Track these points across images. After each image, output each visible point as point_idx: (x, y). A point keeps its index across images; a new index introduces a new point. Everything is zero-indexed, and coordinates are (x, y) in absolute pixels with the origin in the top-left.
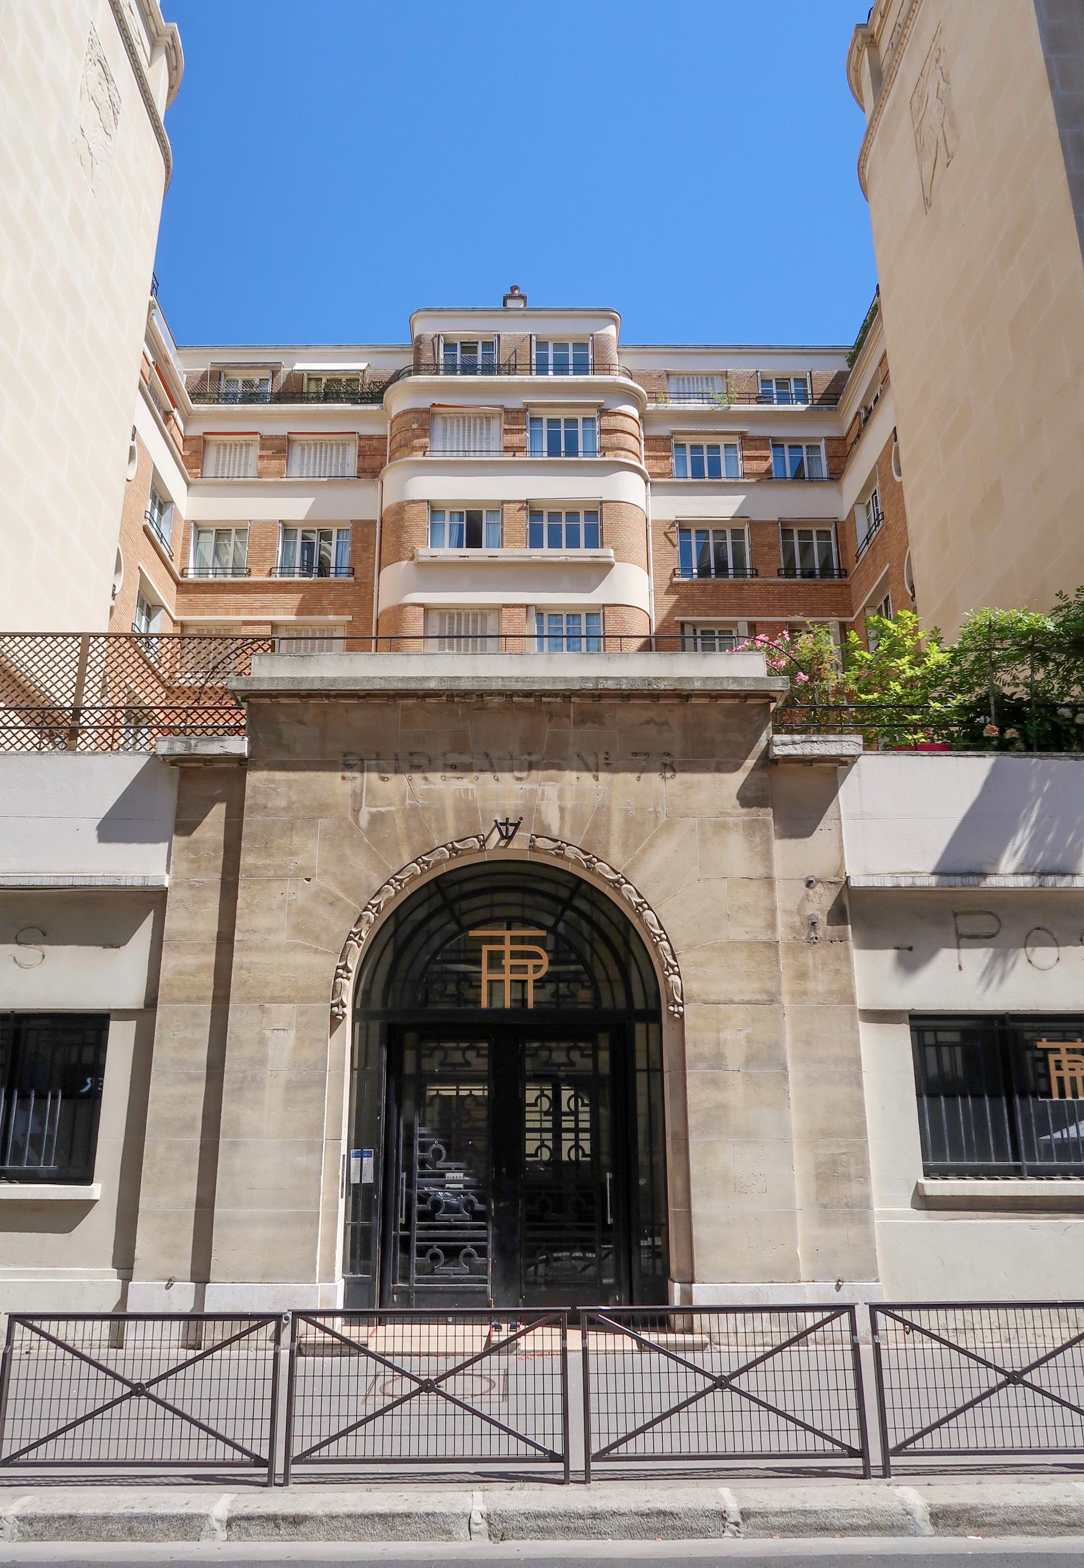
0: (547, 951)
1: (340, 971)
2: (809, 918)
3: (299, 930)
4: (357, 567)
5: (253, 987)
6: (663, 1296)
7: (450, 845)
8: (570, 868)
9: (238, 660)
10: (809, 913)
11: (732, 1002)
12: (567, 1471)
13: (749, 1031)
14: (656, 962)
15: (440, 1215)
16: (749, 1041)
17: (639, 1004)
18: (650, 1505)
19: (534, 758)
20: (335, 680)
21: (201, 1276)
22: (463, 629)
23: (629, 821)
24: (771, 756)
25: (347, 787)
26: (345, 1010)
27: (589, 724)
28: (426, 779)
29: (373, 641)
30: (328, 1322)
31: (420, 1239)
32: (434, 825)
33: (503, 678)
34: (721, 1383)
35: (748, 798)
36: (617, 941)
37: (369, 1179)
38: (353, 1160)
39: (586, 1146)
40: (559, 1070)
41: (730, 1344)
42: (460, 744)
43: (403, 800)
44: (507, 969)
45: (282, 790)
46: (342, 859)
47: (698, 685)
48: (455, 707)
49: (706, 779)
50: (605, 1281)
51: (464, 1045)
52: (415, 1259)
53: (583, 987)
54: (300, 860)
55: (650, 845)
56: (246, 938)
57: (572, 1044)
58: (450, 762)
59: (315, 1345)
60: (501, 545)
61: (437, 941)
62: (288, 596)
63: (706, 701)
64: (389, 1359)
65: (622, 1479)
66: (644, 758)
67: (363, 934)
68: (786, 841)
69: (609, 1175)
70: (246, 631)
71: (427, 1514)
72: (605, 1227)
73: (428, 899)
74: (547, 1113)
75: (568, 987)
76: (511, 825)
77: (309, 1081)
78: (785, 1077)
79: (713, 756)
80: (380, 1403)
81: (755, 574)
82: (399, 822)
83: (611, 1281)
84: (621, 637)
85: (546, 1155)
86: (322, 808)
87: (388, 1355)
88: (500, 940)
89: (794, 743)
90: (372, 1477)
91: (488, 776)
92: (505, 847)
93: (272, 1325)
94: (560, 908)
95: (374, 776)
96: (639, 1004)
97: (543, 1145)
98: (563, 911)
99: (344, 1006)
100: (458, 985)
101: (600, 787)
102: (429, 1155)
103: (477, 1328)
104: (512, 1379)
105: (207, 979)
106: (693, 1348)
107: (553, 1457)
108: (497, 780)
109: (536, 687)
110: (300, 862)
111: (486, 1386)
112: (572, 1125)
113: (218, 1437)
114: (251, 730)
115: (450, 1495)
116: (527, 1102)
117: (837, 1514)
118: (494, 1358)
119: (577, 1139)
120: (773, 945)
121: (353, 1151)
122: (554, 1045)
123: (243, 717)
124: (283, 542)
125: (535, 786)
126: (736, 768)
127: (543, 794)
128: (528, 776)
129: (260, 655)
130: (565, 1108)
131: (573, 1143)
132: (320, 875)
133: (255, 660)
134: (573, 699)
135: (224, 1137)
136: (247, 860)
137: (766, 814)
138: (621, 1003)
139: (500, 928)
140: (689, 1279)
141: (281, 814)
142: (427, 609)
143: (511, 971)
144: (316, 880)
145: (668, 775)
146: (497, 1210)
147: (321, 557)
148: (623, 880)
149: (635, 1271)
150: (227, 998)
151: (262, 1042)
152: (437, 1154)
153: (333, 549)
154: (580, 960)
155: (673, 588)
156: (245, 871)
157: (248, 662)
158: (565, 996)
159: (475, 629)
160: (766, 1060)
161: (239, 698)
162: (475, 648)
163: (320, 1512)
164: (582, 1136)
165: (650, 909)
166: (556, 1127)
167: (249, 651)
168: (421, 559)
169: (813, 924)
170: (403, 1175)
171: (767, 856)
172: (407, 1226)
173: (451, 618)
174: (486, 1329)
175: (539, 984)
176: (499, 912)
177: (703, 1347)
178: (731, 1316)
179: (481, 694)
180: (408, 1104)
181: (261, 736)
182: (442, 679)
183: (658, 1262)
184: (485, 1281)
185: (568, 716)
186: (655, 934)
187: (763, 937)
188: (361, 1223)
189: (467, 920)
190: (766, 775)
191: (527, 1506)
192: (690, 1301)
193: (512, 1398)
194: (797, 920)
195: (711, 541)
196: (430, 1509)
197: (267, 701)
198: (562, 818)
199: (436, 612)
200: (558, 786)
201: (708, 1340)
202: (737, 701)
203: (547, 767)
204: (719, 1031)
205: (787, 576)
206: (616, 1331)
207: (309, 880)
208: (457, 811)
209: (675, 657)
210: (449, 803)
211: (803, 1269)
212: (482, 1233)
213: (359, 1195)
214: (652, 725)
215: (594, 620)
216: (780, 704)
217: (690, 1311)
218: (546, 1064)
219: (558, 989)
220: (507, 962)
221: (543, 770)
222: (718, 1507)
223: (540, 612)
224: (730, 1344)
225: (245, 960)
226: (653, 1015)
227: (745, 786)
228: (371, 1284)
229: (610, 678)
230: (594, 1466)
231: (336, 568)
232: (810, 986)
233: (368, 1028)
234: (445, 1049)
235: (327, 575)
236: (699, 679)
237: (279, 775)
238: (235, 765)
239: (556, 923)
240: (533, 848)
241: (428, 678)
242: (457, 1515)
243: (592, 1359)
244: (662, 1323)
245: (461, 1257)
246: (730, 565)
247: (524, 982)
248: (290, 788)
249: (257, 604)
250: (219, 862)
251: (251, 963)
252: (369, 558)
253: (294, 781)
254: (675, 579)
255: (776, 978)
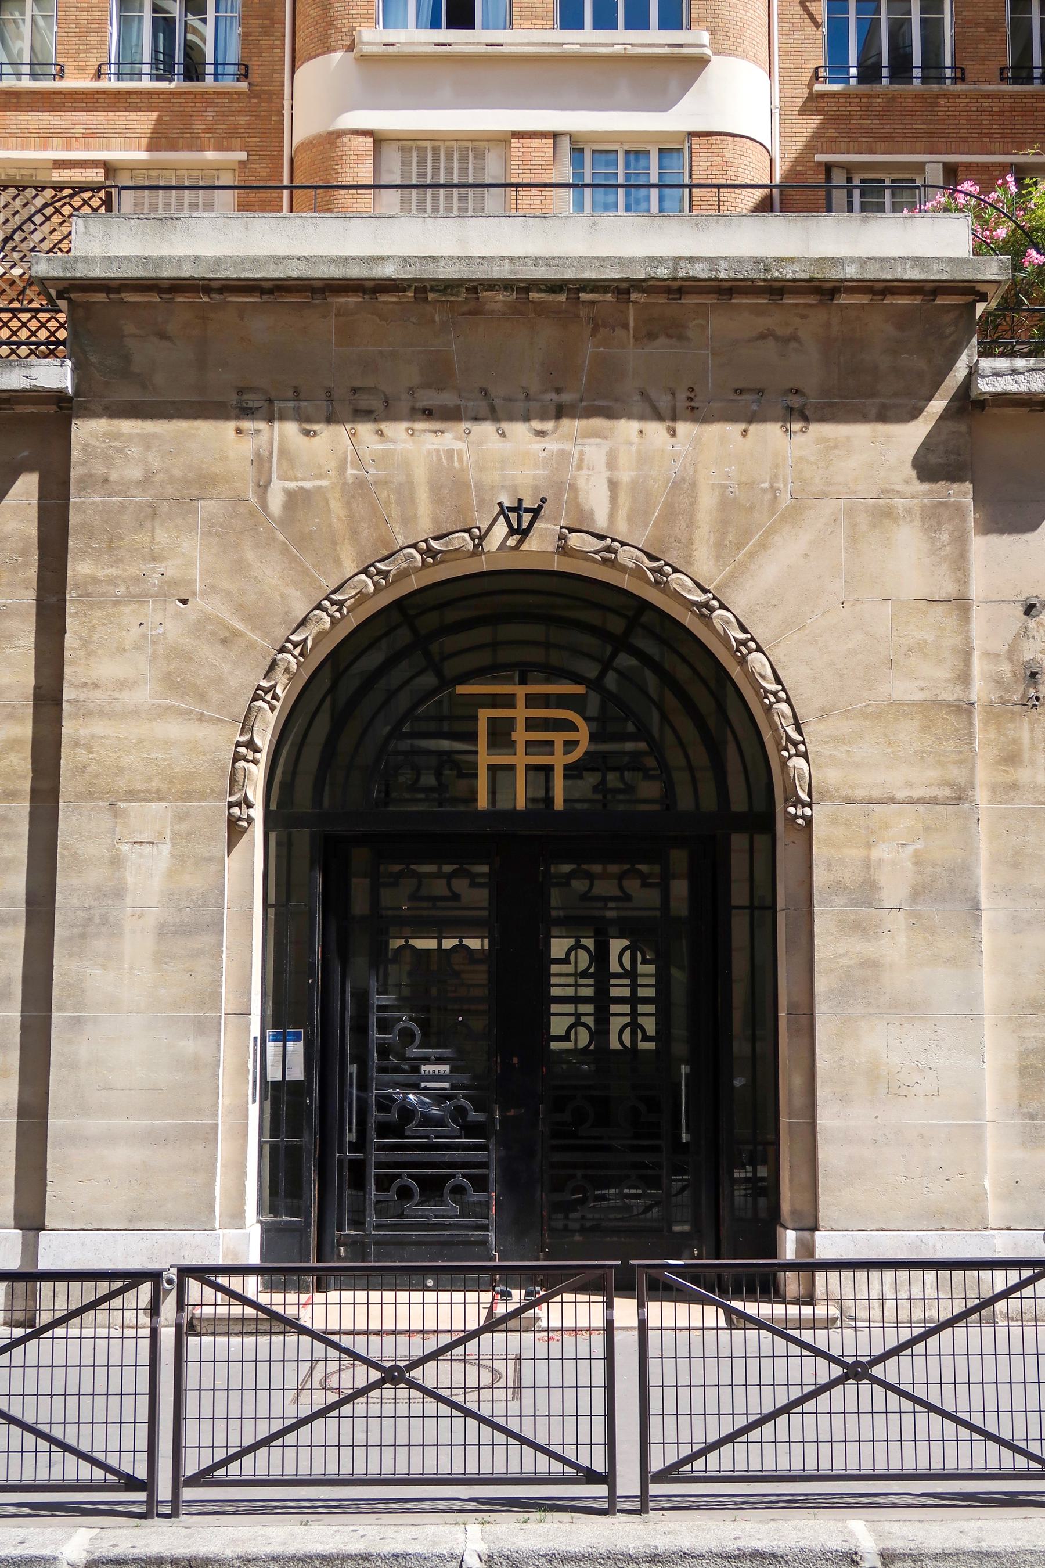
0: (586, 719)
1: (242, 750)
2: (1026, 665)
3: (171, 683)
4: (254, 63)
5: (96, 776)
6: (771, 1247)
7: (423, 545)
8: (626, 582)
9: (47, 227)
10: (1028, 656)
11: (892, 800)
12: (612, 1497)
13: (919, 846)
14: (767, 737)
15: (412, 1128)
16: (918, 861)
17: (739, 803)
18: (740, 1544)
19: (566, 397)
20: (218, 261)
21: (31, 1220)
22: (441, 174)
23: (726, 504)
24: (974, 394)
25: (246, 447)
26: (251, 812)
27: (662, 340)
28: (380, 433)
29: (286, 192)
30: (235, 1283)
31: (378, 1165)
32: (395, 511)
33: (511, 259)
34: (856, 1371)
35: (931, 466)
36: (705, 703)
37: (296, 1073)
38: (271, 1046)
39: (650, 1025)
40: (605, 908)
41: (869, 1315)
42: (438, 373)
43: (342, 469)
44: (520, 748)
45: (135, 450)
46: (240, 567)
47: (851, 272)
48: (429, 308)
49: (860, 432)
50: (677, 1228)
51: (447, 868)
52: (374, 1194)
53: (647, 777)
54: (171, 569)
55: (763, 545)
56: (82, 697)
57: (626, 867)
58: (420, 405)
59: (215, 1320)
60: (508, 24)
61: (403, 701)
62: (133, 115)
63: (865, 299)
64: (335, 1338)
65: (699, 1508)
66: (755, 398)
67: (279, 690)
68: (995, 539)
69: (684, 1069)
70: (59, 176)
71: (396, 1556)
72: (679, 1147)
73: (386, 634)
74: (584, 974)
75: (622, 778)
76: (527, 510)
77: (194, 924)
78: (977, 919)
79: (873, 395)
80: (319, 1399)
81: (961, 77)
82: (337, 507)
83: (686, 1228)
84: (719, 186)
85: (583, 1038)
86: (204, 482)
87: (333, 1333)
88: (508, 701)
89: (1014, 372)
90: (308, 1504)
91: (487, 428)
92: (517, 547)
93: (146, 1288)
94: (609, 649)
95: (291, 428)
96: (739, 803)
97: (578, 1023)
98: (614, 655)
99: (250, 806)
100: (439, 775)
101: (678, 447)
102: (393, 1037)
103: (472, 1296)
104: (527, 1366)
105: (21, 762)
106: (813, 1325)
107: (591, 1477)
108: (503, 435)
109: (570, 274)
110: (170, 573)
111: (486, 1378)
112: (626, 992)
113: (66, 1448)
114: (76, 348)
115: (430, 1530)
116: (553, 955)
117: (1029, 1557)
118: (500, 1337)
119: (634, 1014)
120: (964, 710)
121: (270, 1032)
122: (597, 868)
123: (62, 325)
124: (120, 17)
125: (568, 446)
126: (913, 414)
127: (581, 460)
128: (555, 429)
129: (86, 217)
130: (615, 967)
131: (628, 1019)
132: (204, 593)
133: (77, 225)
134: (634, 296)
135: (59, 1010)
136: (80, 568)
137: (962, 494)
138: (709, 802)
139: (509, 680)
140: (810, 1224)
141: (133, 492)
142: (378, 140)
143: (527, 751)
144: (198, 603)
145: (796, 426)
146: (504, 1120)
147: (189, 46)
148: (715, 603)
149: (724, 1213)
150: (54, 794)
151: (116, 862)
152: (407, 1035)
153: (209, 31)
154: (643, 733)
155: (814, 102)
156: (77, 587)
157: (65, 229)
158: (616, 791)
159: (449, 172)
160: (946, 893)
161: (53, 292)
162: (421, 207)
163: (229, 1553)
164: (642, 1008)
165: (759, 649)
166: (600, 996)
167: (67, 210)
168: (367, 49)
169: (1033, 675)
170: (353, 1069)
171: (960, 563)
172: (360, 1145)
173: (422, 157)
174: (487, 1297)
175: (572, 771)
176: (508, 655)
177: (829, 1324)
178: (875, 1275)
179: (475, 287)
180: (360, 963)
181: (93, 359)
182: (405, 260)
183: (762, 1202)
184: (485, 1228)
185: (626, 326)
186: (767, 691)
187: (950, 695)
188: (285, 1140)
189: (451, 668)
190: (963, 428)
191: (551, 1545)
192: (812, 1254)
193: (527, 1393)
194: (1006, 667)
195: (884, 17)
196: (399, 1549)
197: (101, 297)
198: (613, 499)
199: (394, 146)
200: (606, 445)
201: (838, 1313)
202: (918, 300)
203: (589, 413)
204: (869, 846)
205: (1016, 80)
206: (691, 1298)
207: (184, 602)
208: (435, 489)
209: (814, 221)
210: (421, 474)
211: (994, 1210)
212: (480, 1156)
213: (280, 1099)
214: (771, 343)
215: (672, 160)
216: (994, 304)
217: (809, 1266)
218: (585, 897)
219: (603, 781)
220: (520, 736)
221: (580, 417)
222: (846, 1547)
223: (578, 146)
224: (869, 1315)
225: (82, 732)
226: (761, 821)
227: (927, 446)
228: (302, 1231)
229: (699, 259)
230: (654, 1489)
231: (216, 64)
232: (1024, 775)
233: (290, 843)
234: (420, 876)
235: (199, 77)
236: (853, 260)
237: (128, 426)
238: (52, 409)
239: (603, 674)
240: (563, 550)
241: (382, 258)
242: (441, 1558)
243: (653, 1337)
244: (766, 1287)
245: (446, 1191)
246: (917, 59)
247: (548, 769)
248: (148, 448)
249: (79, 130)
250: (32, 572)
251: (93, 736)
252: (272, 47)
253: (155, 436)
254: (818, 87)
255: (968, 762)
